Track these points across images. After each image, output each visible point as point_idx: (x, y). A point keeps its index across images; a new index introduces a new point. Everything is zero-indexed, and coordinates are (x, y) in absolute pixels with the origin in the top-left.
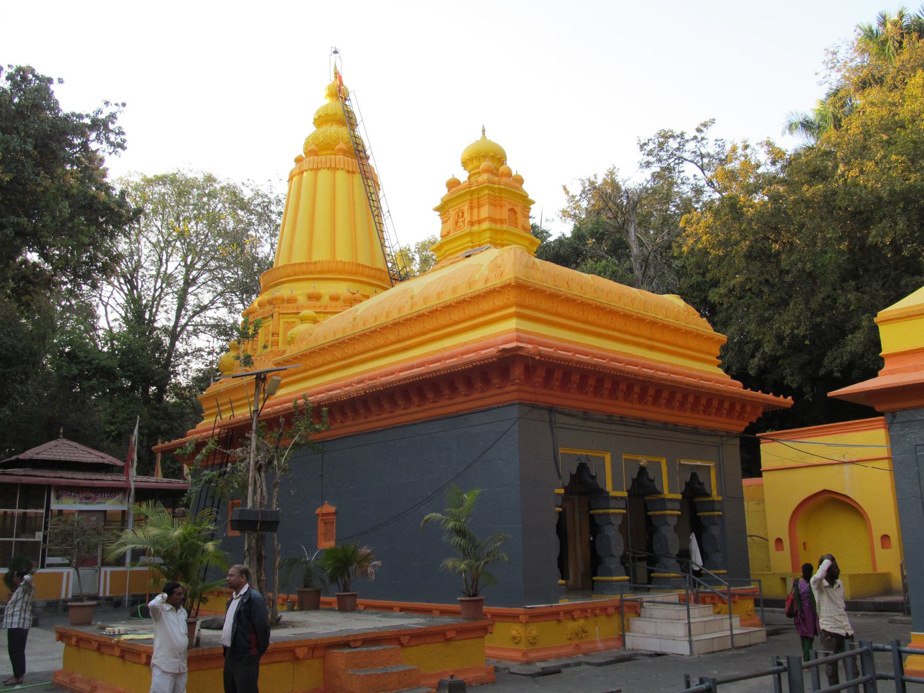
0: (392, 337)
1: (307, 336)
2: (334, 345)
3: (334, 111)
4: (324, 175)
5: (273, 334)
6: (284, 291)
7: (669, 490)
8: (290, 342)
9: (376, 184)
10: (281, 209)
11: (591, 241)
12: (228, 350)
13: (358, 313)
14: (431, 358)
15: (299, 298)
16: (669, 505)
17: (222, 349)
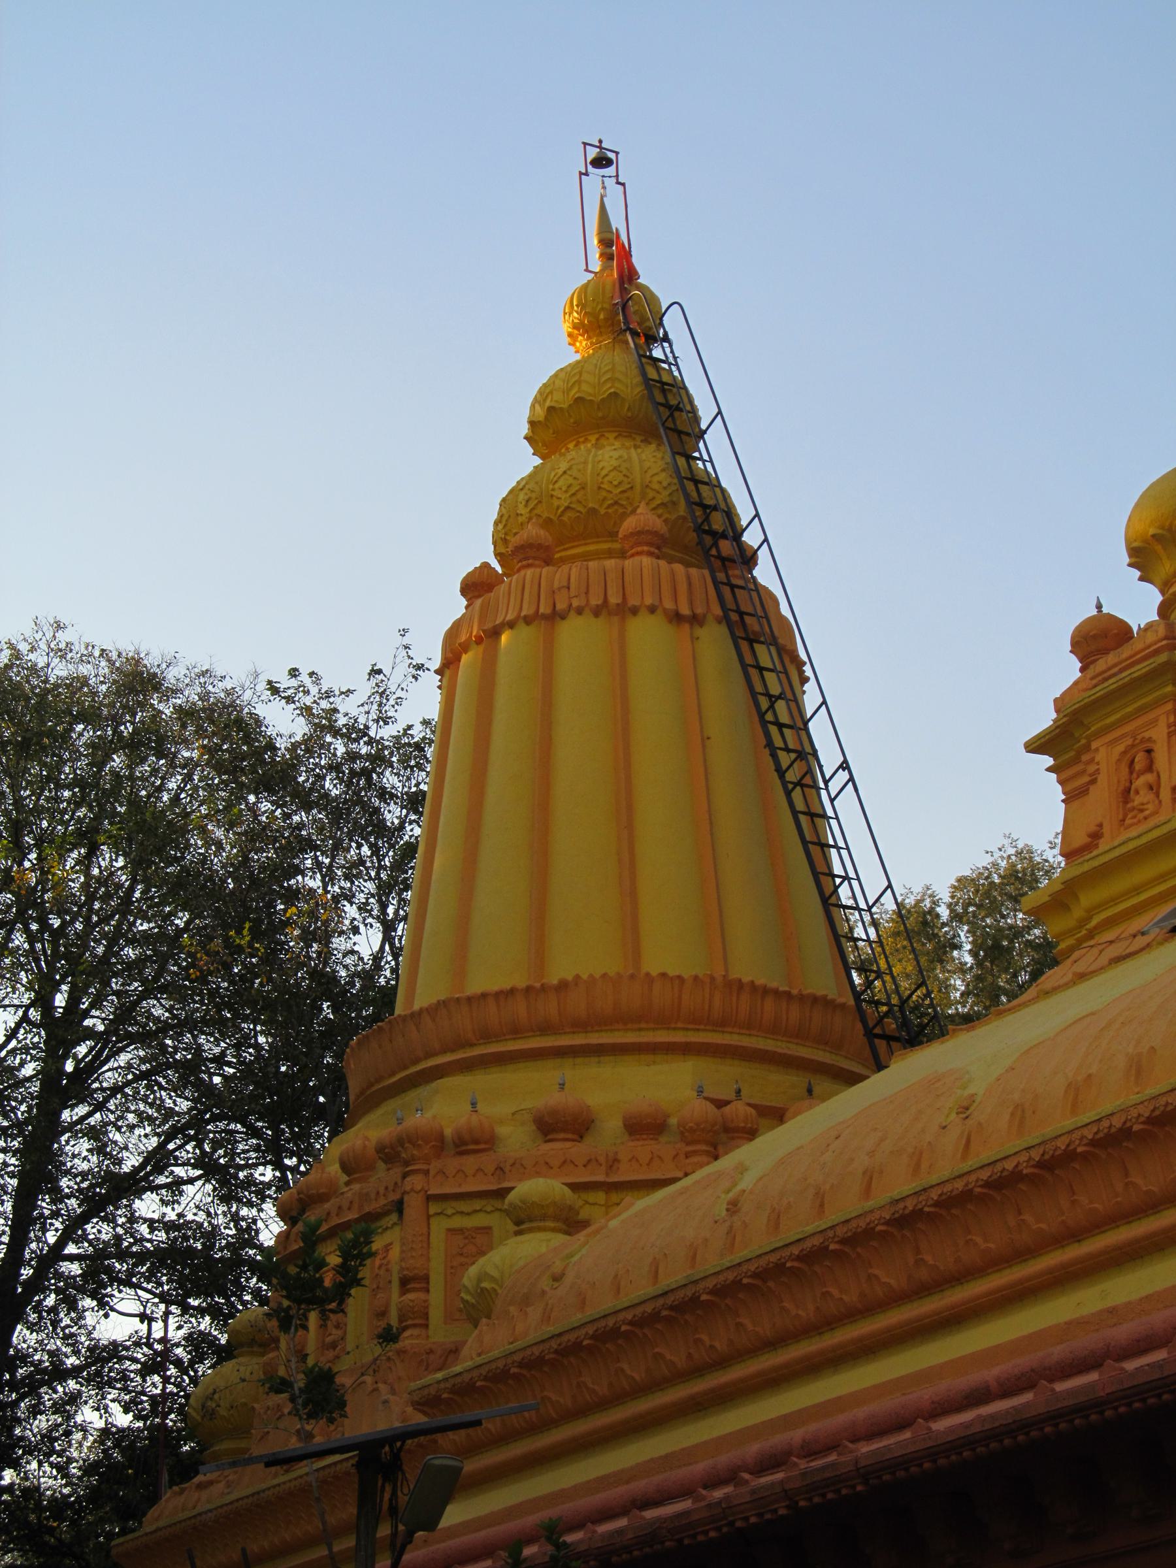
0: (889, 1274)
1: (545, 1283)
2: (655, 1317)
3: (608, 389)
4: (579, 639)
5: (405, 1283)
6: (444, 1107)
8: (478, 1309)
9: (792, 666)
10: (422, 781)
11: (158, 782)
12: (224, 1354)
13: (747, 1182)
14: (1057, 1352)
15: (502, 1131)
17: (198, 1343)
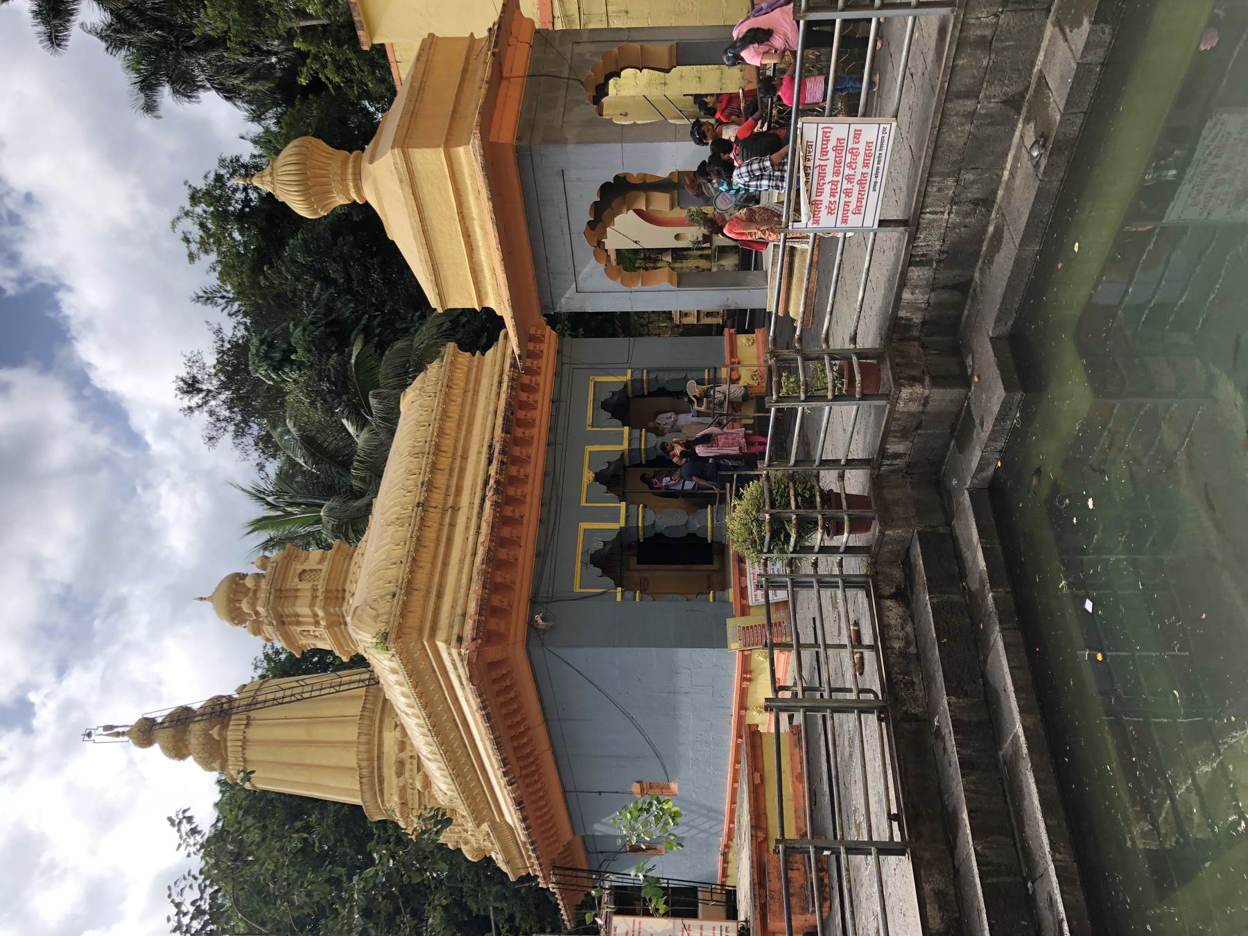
7: (620, 441)
16: (635, 446)
